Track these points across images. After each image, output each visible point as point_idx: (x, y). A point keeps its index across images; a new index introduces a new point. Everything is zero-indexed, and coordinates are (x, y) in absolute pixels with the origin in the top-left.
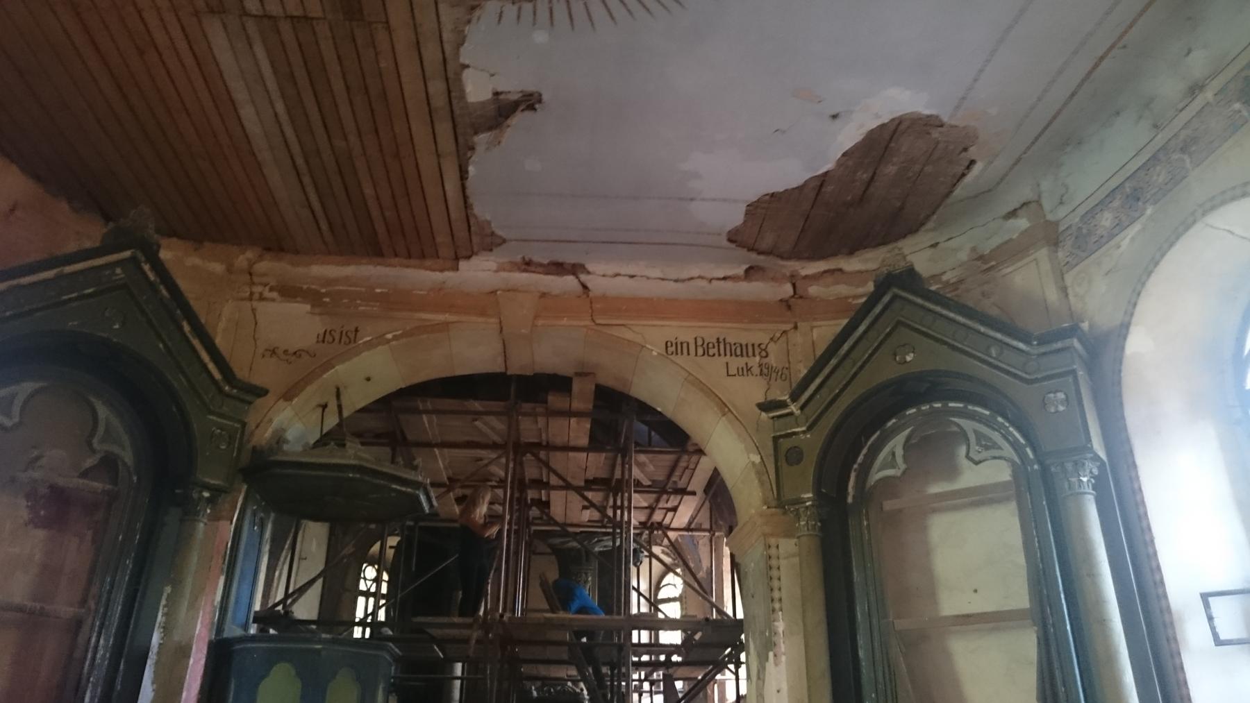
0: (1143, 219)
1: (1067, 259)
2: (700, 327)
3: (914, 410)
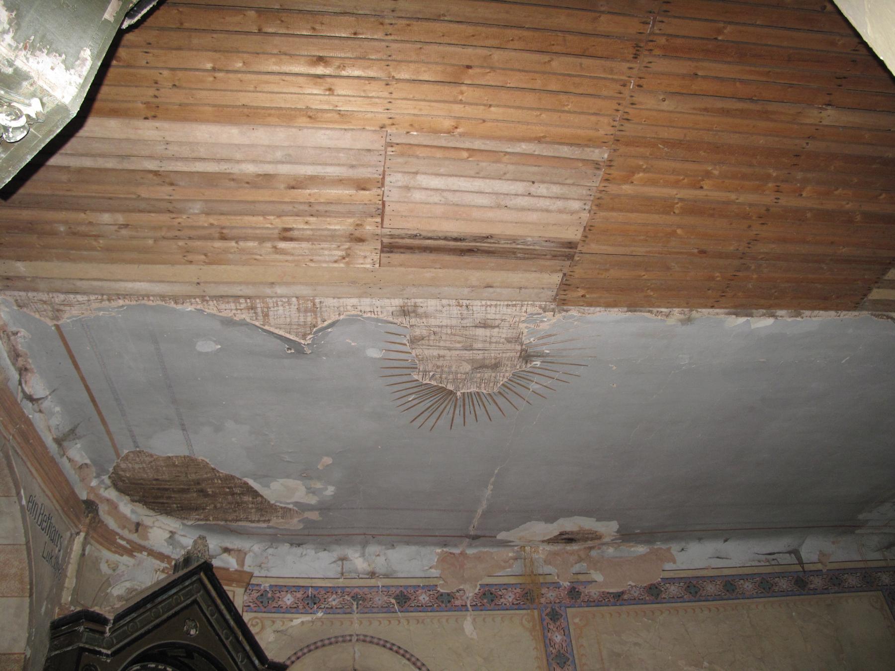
0: (314, 617)
1: (251, 604)
3: (153, 665)
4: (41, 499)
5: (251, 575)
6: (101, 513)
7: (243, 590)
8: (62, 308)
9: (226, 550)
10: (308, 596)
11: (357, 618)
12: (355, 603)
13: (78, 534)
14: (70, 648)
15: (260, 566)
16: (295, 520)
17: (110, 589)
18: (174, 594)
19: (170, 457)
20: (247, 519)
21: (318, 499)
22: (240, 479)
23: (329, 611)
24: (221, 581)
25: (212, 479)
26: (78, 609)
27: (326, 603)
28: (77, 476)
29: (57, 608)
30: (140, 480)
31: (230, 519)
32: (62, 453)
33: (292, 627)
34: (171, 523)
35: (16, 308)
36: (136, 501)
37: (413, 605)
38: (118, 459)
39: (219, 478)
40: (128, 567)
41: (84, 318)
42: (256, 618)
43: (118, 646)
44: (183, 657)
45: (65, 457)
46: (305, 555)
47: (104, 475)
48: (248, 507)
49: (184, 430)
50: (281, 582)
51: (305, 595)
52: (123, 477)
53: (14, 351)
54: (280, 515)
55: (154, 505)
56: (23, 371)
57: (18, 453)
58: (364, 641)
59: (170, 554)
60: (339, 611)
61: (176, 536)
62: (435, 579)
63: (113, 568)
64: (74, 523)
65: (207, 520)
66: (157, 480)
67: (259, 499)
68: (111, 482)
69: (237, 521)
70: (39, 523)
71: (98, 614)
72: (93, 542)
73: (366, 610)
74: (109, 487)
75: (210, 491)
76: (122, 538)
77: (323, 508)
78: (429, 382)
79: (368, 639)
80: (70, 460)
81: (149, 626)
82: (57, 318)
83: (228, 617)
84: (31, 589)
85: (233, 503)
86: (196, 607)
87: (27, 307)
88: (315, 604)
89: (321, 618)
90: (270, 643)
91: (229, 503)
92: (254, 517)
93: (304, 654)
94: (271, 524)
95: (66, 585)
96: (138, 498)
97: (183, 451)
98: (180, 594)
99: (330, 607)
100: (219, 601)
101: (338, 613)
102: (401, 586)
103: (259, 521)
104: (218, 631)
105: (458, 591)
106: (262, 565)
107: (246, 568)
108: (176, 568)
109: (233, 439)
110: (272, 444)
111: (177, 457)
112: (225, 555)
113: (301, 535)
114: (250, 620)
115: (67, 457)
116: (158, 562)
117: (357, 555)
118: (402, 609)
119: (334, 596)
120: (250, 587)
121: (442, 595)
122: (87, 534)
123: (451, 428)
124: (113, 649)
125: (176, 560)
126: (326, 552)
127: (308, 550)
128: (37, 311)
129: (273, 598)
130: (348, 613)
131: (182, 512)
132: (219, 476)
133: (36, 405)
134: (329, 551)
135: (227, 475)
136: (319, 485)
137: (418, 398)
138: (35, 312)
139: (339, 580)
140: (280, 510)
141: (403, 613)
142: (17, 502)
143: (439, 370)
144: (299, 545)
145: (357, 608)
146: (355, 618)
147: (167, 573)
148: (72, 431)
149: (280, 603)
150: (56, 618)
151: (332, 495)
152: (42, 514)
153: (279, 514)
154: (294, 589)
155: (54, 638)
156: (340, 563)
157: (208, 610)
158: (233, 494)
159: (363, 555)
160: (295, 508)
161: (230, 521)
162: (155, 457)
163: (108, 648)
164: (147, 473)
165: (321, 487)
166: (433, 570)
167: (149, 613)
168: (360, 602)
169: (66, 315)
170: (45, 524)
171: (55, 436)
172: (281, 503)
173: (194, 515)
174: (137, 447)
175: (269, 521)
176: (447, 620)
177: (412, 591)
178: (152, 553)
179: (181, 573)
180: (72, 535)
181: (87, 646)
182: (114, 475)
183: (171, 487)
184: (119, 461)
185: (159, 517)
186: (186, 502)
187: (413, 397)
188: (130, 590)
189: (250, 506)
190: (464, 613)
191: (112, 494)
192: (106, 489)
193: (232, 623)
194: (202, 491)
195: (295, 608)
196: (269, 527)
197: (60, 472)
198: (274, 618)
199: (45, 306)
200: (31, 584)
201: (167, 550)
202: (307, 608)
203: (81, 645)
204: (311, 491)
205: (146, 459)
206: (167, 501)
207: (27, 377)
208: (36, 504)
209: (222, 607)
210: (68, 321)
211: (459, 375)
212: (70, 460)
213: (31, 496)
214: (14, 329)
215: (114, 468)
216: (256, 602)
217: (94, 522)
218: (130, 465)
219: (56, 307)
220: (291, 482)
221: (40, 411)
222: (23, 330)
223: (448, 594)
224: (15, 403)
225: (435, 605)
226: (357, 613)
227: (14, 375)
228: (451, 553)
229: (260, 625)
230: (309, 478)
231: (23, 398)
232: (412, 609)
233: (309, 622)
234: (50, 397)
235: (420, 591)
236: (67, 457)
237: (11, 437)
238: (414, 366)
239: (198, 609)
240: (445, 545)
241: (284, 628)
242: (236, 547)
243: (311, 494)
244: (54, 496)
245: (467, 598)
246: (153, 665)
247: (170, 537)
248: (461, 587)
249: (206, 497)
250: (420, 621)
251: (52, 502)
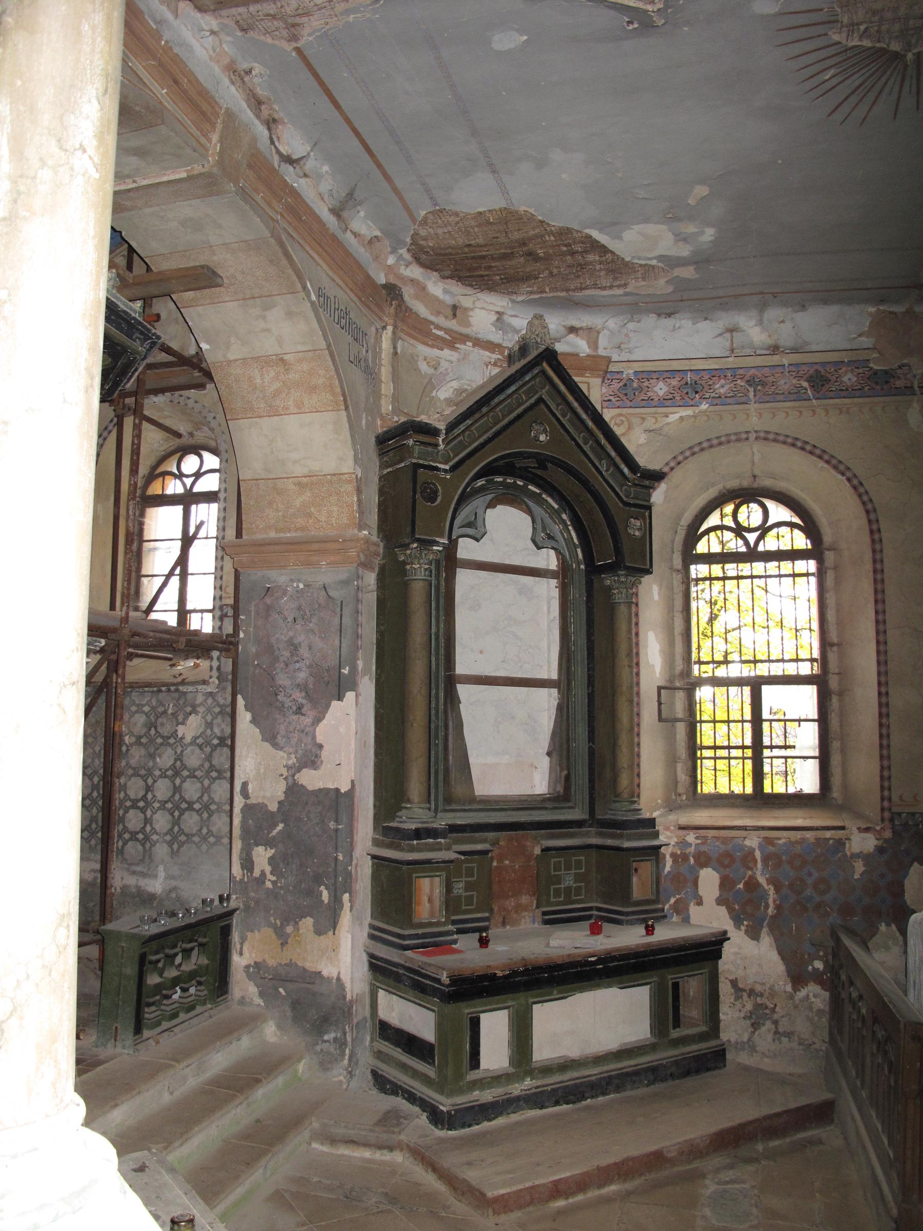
0: (697, 410)
1: (611, 398)
2: (413, 1088)
3: (501, 479)
4: (332, 291)
5: (609, 360)
6: (406, 298)
7: (599, 380)
8: (298, 20)
9: (572, 330)
10: (687, 383)
11: (756, 409)
12: (751, 390)
13: (384, 328)
14: (403, 465)
15: (619, 347)
16: (662, 282)
17: (435, 391)
18: (514, 392)
19: (480, 213)
20: (595, 286)
21: (691, 249)
22: (581, 232)
23: (716, 401)
24: (569, 371)
25: (542, 236)
26: (403, 419)
27: (712, 391)
28: (368, 254)
29: (300, 1071)
30: (448, 248)
31: (572, 288)
32: (344, 227)
33: (668, 424)
34: (496, 302)
35: (239, 34)
36: (447, 278)
37: (834, 389)
38: (415, 225)
39: (551, 233)
40: (452, 363)
41: (330, 29)
42: (621, 415)
43: (457, 459)
44: (534, 468)
45: (348, 231)
46: (679, 328)
47: (401, 249)
48: (595, 269)
49: (494, 172)
50: (649, 367)
51: (683, 382)
52: (424, 247)
53: (254, 98)
54: (640, 276)
55: (470, 279)
56: (271, 123)
57: (292, 236)
58: (766, 439)
59: (501, 341)
60: (729, 401)
61: (505, 317)
62: (867, 351)
63: (433, 366)
64: (376, 315)
65: (541, 292)
66: (469, 245)
67: (609, 256)
68: (412, 256)
69: (582, 289)
70: (336, 321)
71: (427, 424)
72: (403, 336)
73: (766, 398)
74: (410, 263)
75: (541, 252)
76: (438, 327)
77: (700, 260)
78: (858, 43)
79: (771, 436)
80: (356, 235)
81: (489, 434)
82: (294, 38)
83: (584, 416)
84: (345, 400)
85: (574, 266)
86: (542, 406)
87: (253, 29)
88: (697, 392)
89: (705, 411)
90: (641, 445)
91: (569, 266)
92: (605, 282)
93: (687, 458)
94: (627, 290)
95: (383, 392)
96: (450, 272)
97: (496, 202)
98: (520, 392)
99: (717, 396)
100: (570, 398)
101: (730, 404)
102: (816, 363)
103: (611, 287)
104: (574, 435)
105: (900, 367)
106: (622, 346)
107: (601, 352)
108: (511, 359)
109: (563, 176)
110: (620, 175)
111: (489, 211)
112: (572, 337)
113: (671, 301)
114: (612, 418)
115: (351, 231)
116: (487, 353)
117: (753, 323)
118: (817, 396)
119: (723, 381)
120: (609, 376)
121: (875, 374)
122: (395, 327)
123: (895, 118)
124: (451, 464)
125: (510, 349)
126: (707, 321)
127: (683, 322)
128: (267, 32)
129: (640, 389)
130: (743, 403)
131: (508, 285)
132: (551, 230)
133: (298, 167)
134: (711, 320)
135: (561, 228)
136: (691, 229)
137: (841, 72)
138: (264, 34)
139: (728, 359)
140: (640, 269)
141: (819, 401)
142: (305, 298)
143: (876, 19)
144: (669, 315)
145: (755, 396)
146: (753, 409)
147: (501, 366)
148: (350, 195)
149: (649, 394)
150: (380, 431)
151: (711, 242)
152: (338, 310)
153: (639, 275)
154: (667, 375)
155: (383, 453)
156: (728, 335)
157: (557, 409)
158: (573, 253)
159: (760, 322)
160: (660, 264)
161: (574, 290)
162: (461, 215)
163: (446, 463)
164: (455, 239)
165: (696, 230)
166: (863, 339)
167: (485, 419)
168: (759, 388)
169: (306, 31)
170: (343, 321)
171: (331, 207)
172: (639, 259)
173: (525, 288)
174: (436, 205)
175: (625, 285)
176: (883, 408)
177: (833, 370)
178: (478, 343)
179: (518, 365)
180: (377, 330)
181: (421, 462)
182: (413, 247)
183: (490, 253)
184: (416, 227)
185: (480, 295)
186: (512, 271)
187: (832, 72)
188: (459, 392)
189: (598, 267)
190: (910, 398)
191: (415, 272)
192: (407, 266)
193: (590, 424)
194: (530, 254)
195: (671, 399)
196: (626, 294)
197: (348, 254)
198: (643, 414)
199: (275, 23)
200: (344, 395)
201: (496, 337)
202: (686, 397)
203: (414, 461)
204: (681, 238)
205: (450, 220)
206: (487, 273)
207: (278, 131)
208: (328, 298)
209: (576, 405)
210: (311, 39)
211: (912, 22)
212: (356, 235)
213: (320, 288)
214: (245, 66)
215: (412, 239)
216: (619, 394)
217: (400, 311)
218: (431, 230)
219: (290, 20)
220: (651, 229)
221: (305, 175)
222: (256, 64)
223: (886, 372)
224: (273, 171)
225: (866, 388)
226: (755, 403)
227: (261, 130)
228: (891, 313)
229: (626, 423)
230: (676, 219)
231: (280, 161)
232: (832, 394)
233: (689, 416)
234: (312, 154)
235: (844, 369)
236: (351, 231)
237: (279, 217)
238: (833, 18)
239: (546, 410)
240: (882, 301)
241: (658, 426)
242: (584, 325)
243: (681, 242)
244: (347, 285)
245: (915, 376)
246: (501, 479)
247: (498, 319)
248: (906, 361)
249: (536, 262)
250: (844, 410)
251: (346, 293)
